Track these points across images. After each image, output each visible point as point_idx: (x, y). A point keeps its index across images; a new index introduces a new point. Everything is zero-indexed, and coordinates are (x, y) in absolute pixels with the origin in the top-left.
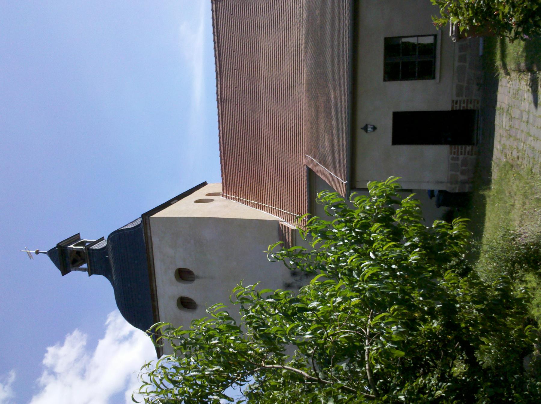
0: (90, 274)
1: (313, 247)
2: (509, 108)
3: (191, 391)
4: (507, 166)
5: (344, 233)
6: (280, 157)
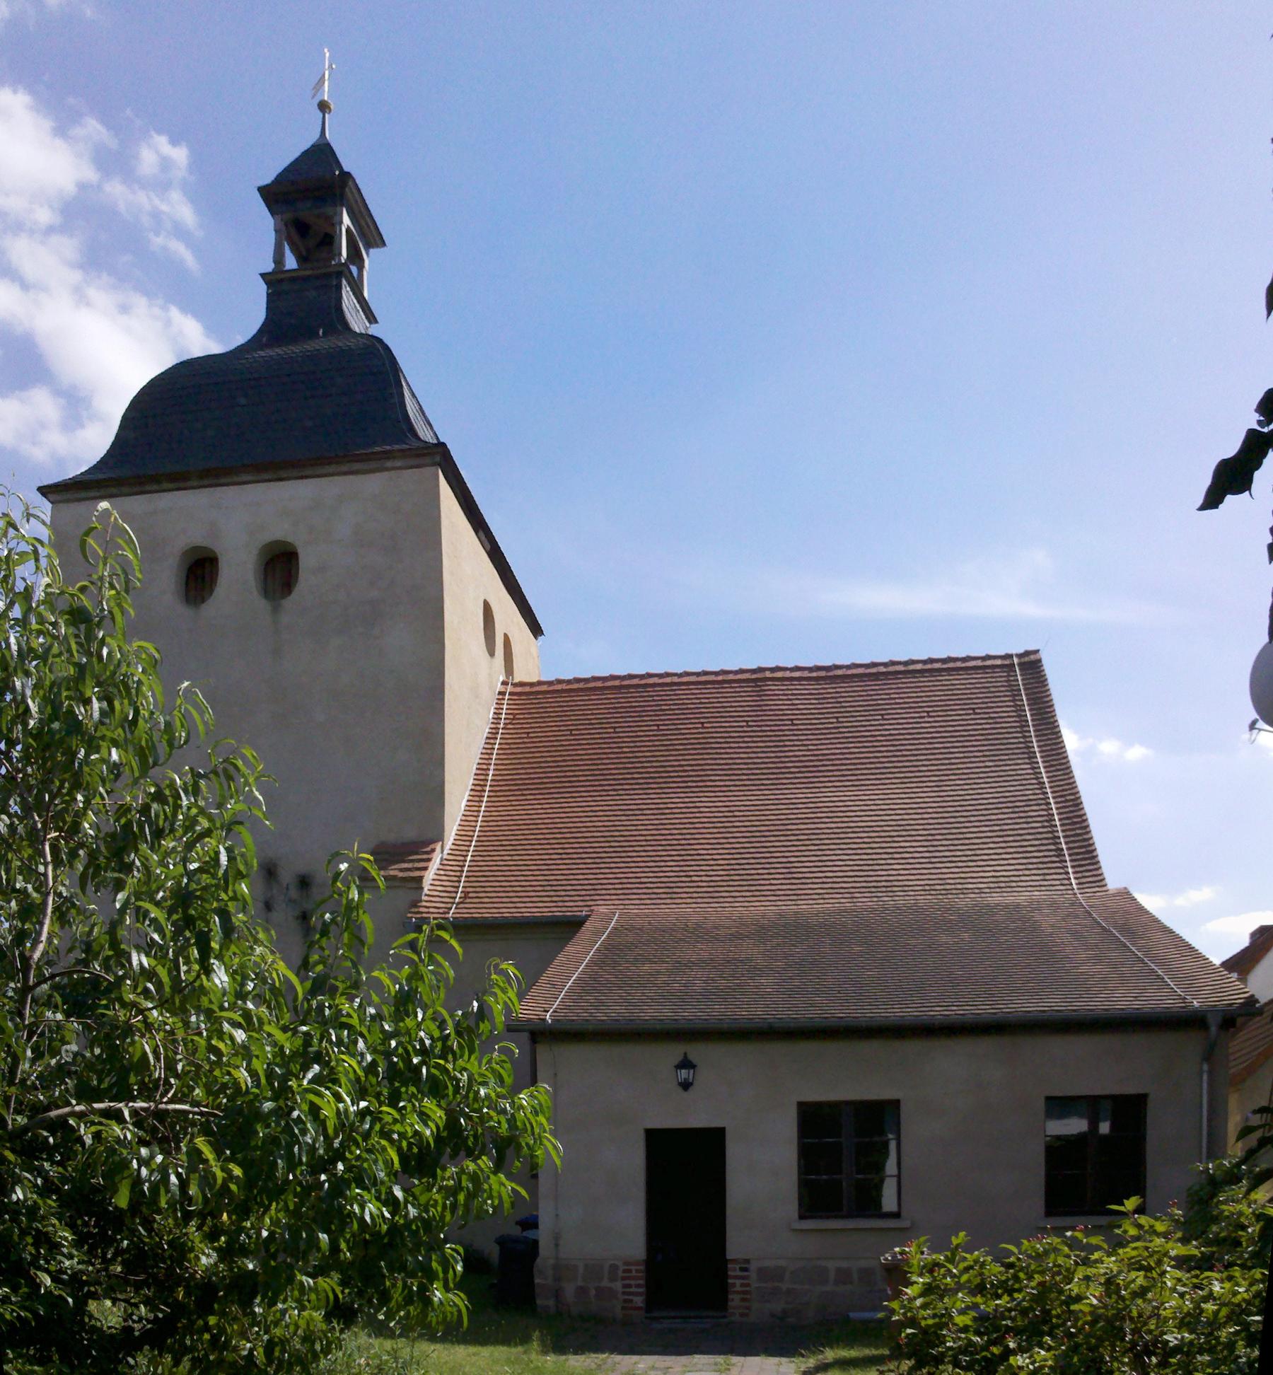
0: (269, 277)
1: (373, 974)
5: (414, 1036)
6: (613, 844)
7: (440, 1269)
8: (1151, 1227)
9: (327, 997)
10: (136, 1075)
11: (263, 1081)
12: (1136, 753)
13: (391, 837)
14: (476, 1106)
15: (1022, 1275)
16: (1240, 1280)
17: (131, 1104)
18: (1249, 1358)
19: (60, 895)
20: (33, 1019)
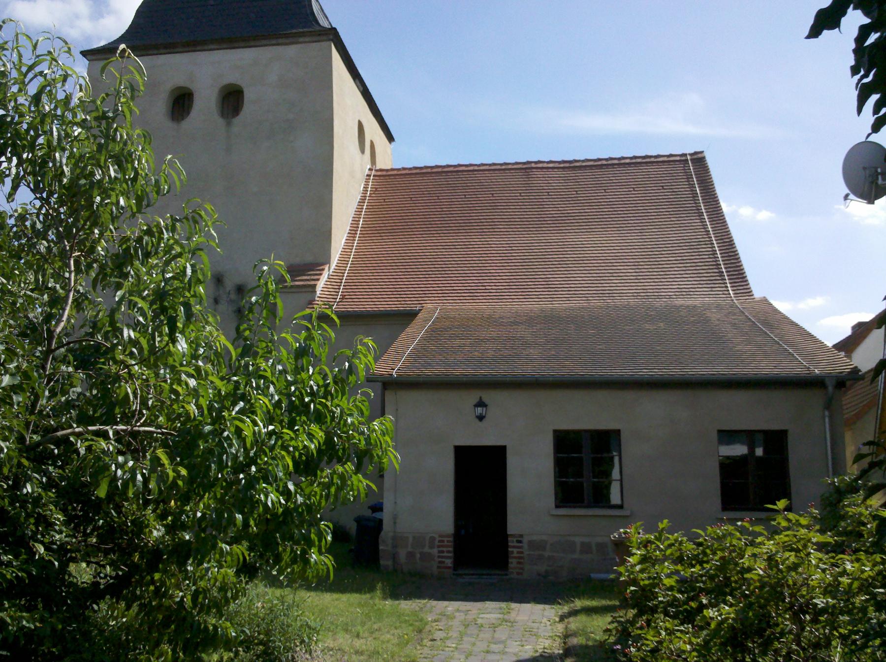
2: (510, 622)
3: (25, 126)
4: (420, 623)
5: (306, 384)
7: (316, 539)
8: (797, 521)
9: (251, 358)
10: (120, 408)
11: (206, 412)
12: (764, 215)
13: (297, 260)
14: (345, 429)
15: (708, 551)
16: (865, 562)
17: (114, 427)
18: (878, 620)
19: (78, 292)
20: (52, 371)
